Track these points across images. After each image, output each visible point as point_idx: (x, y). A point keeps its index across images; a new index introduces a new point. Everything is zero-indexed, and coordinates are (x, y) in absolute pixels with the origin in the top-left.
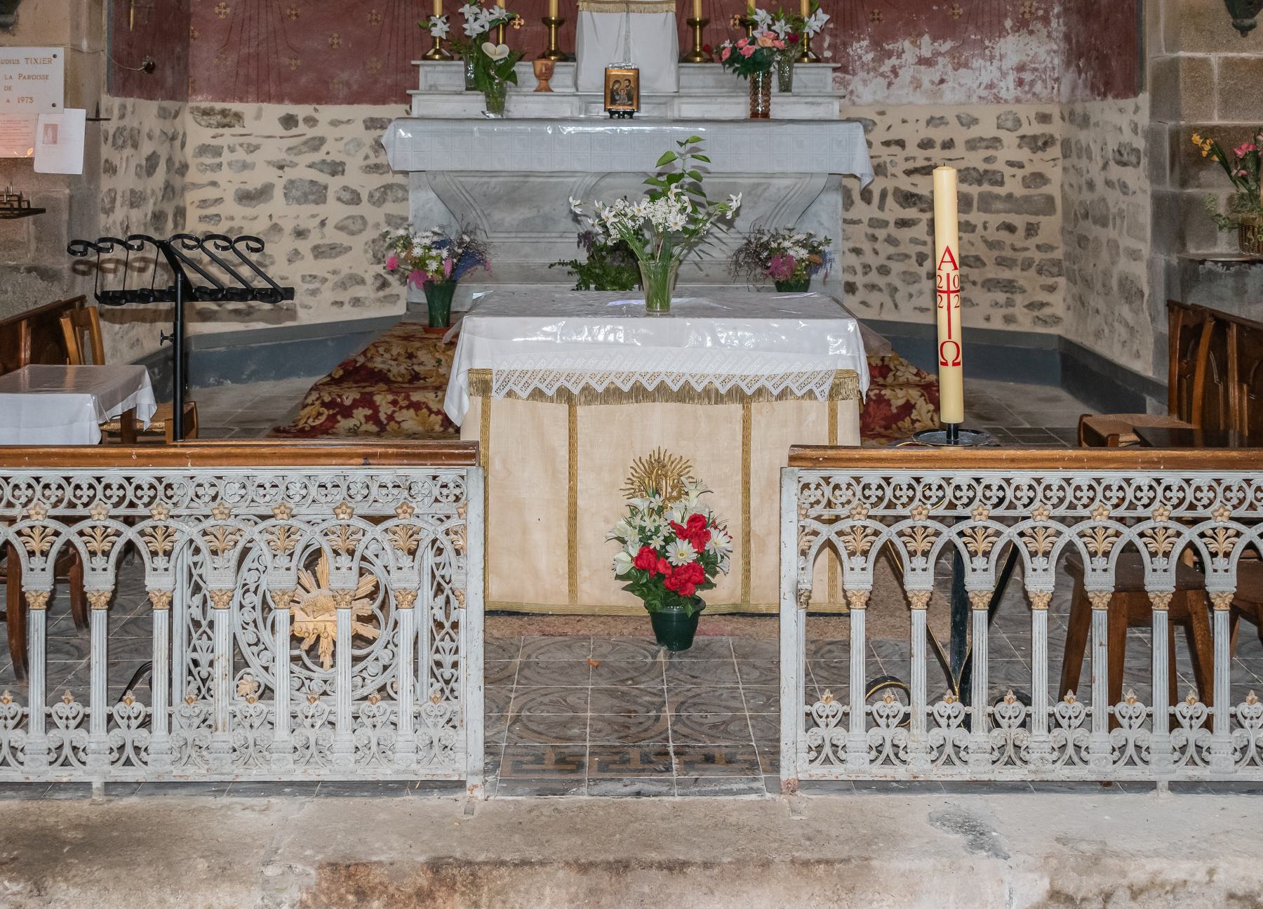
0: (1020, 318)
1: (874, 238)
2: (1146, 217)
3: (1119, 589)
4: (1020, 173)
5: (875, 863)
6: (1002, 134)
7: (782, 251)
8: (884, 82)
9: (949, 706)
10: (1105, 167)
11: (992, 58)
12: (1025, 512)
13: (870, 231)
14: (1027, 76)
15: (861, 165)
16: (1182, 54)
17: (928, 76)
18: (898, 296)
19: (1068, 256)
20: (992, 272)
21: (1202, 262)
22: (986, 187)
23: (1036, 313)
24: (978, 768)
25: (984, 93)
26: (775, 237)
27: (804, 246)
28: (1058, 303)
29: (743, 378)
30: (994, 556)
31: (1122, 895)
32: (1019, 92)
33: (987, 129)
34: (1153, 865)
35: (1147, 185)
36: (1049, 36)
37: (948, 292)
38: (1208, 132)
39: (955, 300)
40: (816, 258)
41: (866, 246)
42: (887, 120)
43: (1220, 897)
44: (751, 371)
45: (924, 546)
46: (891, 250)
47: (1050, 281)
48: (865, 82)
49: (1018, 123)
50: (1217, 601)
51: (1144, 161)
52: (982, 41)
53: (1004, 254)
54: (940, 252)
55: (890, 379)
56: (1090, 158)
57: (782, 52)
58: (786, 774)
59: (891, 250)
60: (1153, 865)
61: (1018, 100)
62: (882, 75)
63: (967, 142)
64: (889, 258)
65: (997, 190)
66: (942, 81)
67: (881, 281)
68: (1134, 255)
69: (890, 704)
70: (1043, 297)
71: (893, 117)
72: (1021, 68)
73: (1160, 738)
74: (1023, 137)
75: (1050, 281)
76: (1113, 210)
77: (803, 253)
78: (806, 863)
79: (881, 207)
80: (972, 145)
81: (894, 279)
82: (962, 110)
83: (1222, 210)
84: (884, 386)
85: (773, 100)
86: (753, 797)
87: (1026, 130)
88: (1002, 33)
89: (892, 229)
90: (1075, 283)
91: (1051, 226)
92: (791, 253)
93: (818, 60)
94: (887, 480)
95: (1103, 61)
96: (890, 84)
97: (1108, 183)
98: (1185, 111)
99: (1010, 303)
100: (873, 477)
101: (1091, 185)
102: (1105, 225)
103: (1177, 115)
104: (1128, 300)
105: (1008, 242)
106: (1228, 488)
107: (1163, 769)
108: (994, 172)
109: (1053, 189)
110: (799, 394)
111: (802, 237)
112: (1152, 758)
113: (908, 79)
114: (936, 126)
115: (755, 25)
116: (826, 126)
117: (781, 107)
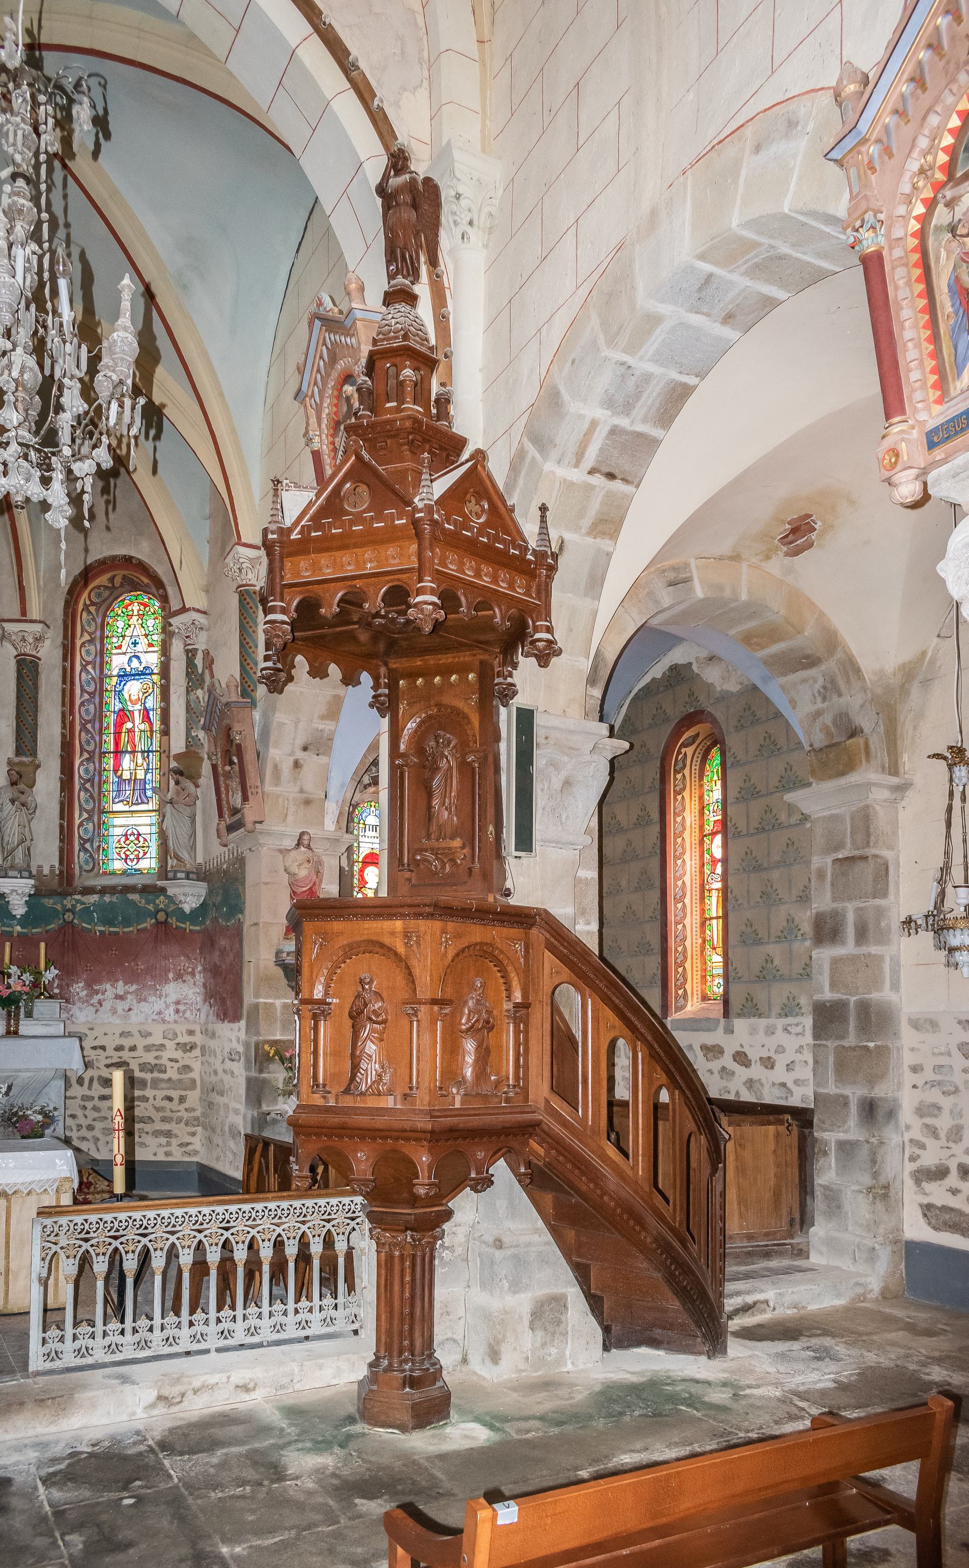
0: (174, 1152)
1: (85, 1108)
2: (242, 1091)
3: (194, 1264)
4: (176, 1065)
5: (76, 1395)
6: (166, 1042)
7: (25, 1117)
8: (94, 1010)
9: (114, 1325)
10: (223, 1062)
11: (160, 996)
12: (152, 1231)
13: (82, 1103)
14: (181, 1008)
15: (76, 1064)
16: (261, 1000)
17: (121, 1006)
18: (99, 1143)
19: (203, 1114)
20: (159, 1126)
21: (269, 1114)
22: (156, 1074)
23: (184, 1149)
24: (128, 1353)
25: (156, 1017)
26: (21, 1108)
27: (40, 1113)
28: (197, 1143)
29: (7, 1185)
30: (137, 1253)
31: (190, 1393)
32: (176, 1017)
33: (157, 1039)
34: (203, 1378)
35: (244, 1073)
36: (194, 984)
37: (119, 1130)
38: (273, 1043)
39: (122, 1134)
40: (48, 1120)
41: (79, 1113)
42: (95, 1033)
43: (232, 1388)
44: (12, 1181)
45: (104, 1250)
46: (96, 1115)
47: (193, 1129)
48: (80, 1009)
49: (176, 1035)
50: (238, 1263)
51: (243, 1059)
52: (155, 985)
53: (165, 1114)
54: (115, 1110)
55: (92, 1189)
56: (215, 1056)
57: (27, 994)
58: (32, 1368)
59: (96, 1115)
60: (203, 1378)
61: (176, 1022)
62: (92, 1005)
63: (145, 1047)
64: (94, 1120)
65: (162, 1076)
66: (130, 1010)
67: (89, 1135)
68: (236, 1112)
69: (85, 1329)
70: (188, 1139)
71: (98, 1032)
72: (178, 1003)
73: (213, 1328)
74: (178, 1044)
75: (193, 1129)
76: (227, 1087)
77: (40, 1118)
78: (42, 1400)
79: (90, 1088)
80: (148, 1049)
81: (97, 1133)
82: (142, 1028)
83: (281, 1086)
84: (88, 1193)
85: (21, 1022)
86: (14, 1382)
87: (180, 1039)
88: (167, 981)
89: (96, 1102)
90: (206, 1130)
91: (193, 1097)
92: (32, 1118)
93: (51, 997)
94: (86, 1221)
95: (223, 1001)
96: (97, 1011)
97: (225, 1071)
98: (262, 1032)
99: (168, 1144)
100: (79, 1219)
101: (216, 1072)
102: (222, 1096)
103: (258, 1033)
104: (233, 1137)
105: (168, 1107)
106: (244, 1212)
107: (213, 1342)
108: (161, 1065)
109: (195, 1075)
110: (39, 1191)
111: (38, 1108)
112: (207, 1338)
113: (109, 1008)
114: (126, 1037)
115: (9, 976)
116: (55, 1040)
117: (26, 1027)
